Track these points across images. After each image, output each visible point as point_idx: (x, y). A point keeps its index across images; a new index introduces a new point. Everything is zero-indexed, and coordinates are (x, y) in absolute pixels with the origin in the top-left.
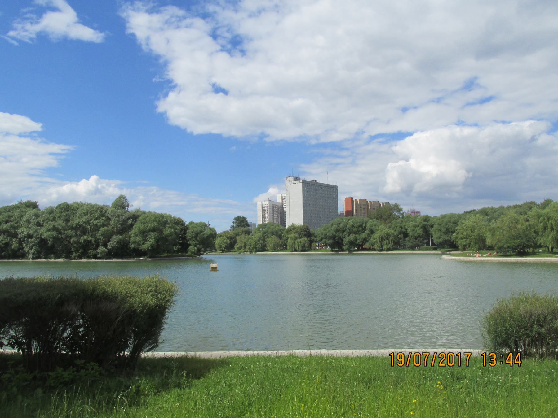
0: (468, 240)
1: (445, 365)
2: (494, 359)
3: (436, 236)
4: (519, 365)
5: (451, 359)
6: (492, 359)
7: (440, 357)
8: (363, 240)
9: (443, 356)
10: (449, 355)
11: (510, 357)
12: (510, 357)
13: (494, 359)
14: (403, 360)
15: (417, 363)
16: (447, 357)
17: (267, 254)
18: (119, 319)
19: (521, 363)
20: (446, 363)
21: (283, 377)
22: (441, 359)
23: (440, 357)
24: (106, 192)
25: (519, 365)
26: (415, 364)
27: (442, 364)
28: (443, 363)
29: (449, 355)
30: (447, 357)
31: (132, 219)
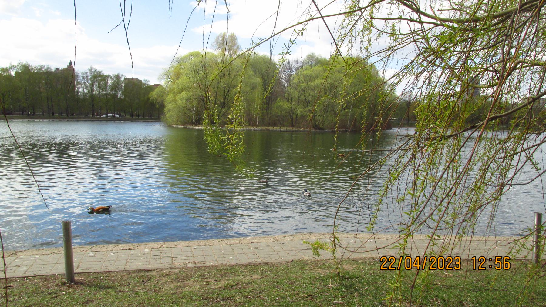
0: (252, 72)
2: (458, 263)
3: (44, 151)
4: (418, 269)
6: (457, 263)
7: (430, 260)
8: (312, 62)
9: (384, 260)
10: (439, 258)
11: (417, 261)
12: (417, 261)
13: (458, 263)
14: (505, 263)
15: (441, 266)
19: (419, 267)
23: (430, 260)
24: (44, 70)
25: (418, 269)
26: (406, 268)
27: (481, 267)
28: (483, 266)
29: (439, 258)
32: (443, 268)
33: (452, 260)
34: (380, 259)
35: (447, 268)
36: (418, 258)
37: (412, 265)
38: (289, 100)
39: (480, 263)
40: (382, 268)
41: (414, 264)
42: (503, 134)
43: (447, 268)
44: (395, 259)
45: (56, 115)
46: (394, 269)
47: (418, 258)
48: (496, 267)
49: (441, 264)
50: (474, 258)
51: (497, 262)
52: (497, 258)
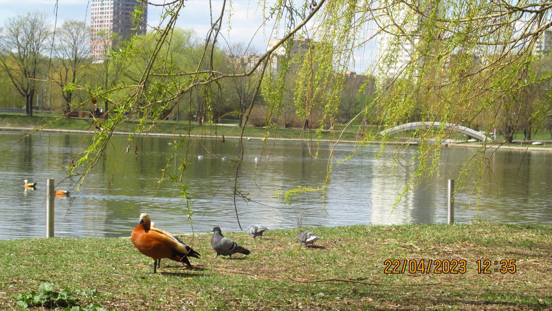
1: (457, 272)
2: (464, 267)
5: (413, 267)
6: (503, 266)
7: (435, 264)
9: (396, 263)
10: (444, 262)
11: (422, 264)
12: (422, 264)
15: (413, 270)
16: (442, 263)
17: (56, 132)
18: (142, 179)
19: (424, 270)
20: (458, 270)
21: (392, 295)
22: (435, 266)
23: (435, 264)
27: (486, 271)
29: (444, 262)
30: (442, 263)
31: (101, 111)
32: (448, 271)
33: (415, 262)
34: (385, 262)
35: (452, 272)
36: (422, 261)
37: (417, 268)
38: (531, 102)
39: (435, 266)
40: (386, 272)
41: (419, 268)
42: (109, 11)
43: (452, 272)
44: (466, 262)
45: (146, 13)
46: (399, 272)
47: (422, 261)
48: (501, 271)
49: (413, 265)
50: (479, 262)
51: (510, 265)
52: (511, 261)
